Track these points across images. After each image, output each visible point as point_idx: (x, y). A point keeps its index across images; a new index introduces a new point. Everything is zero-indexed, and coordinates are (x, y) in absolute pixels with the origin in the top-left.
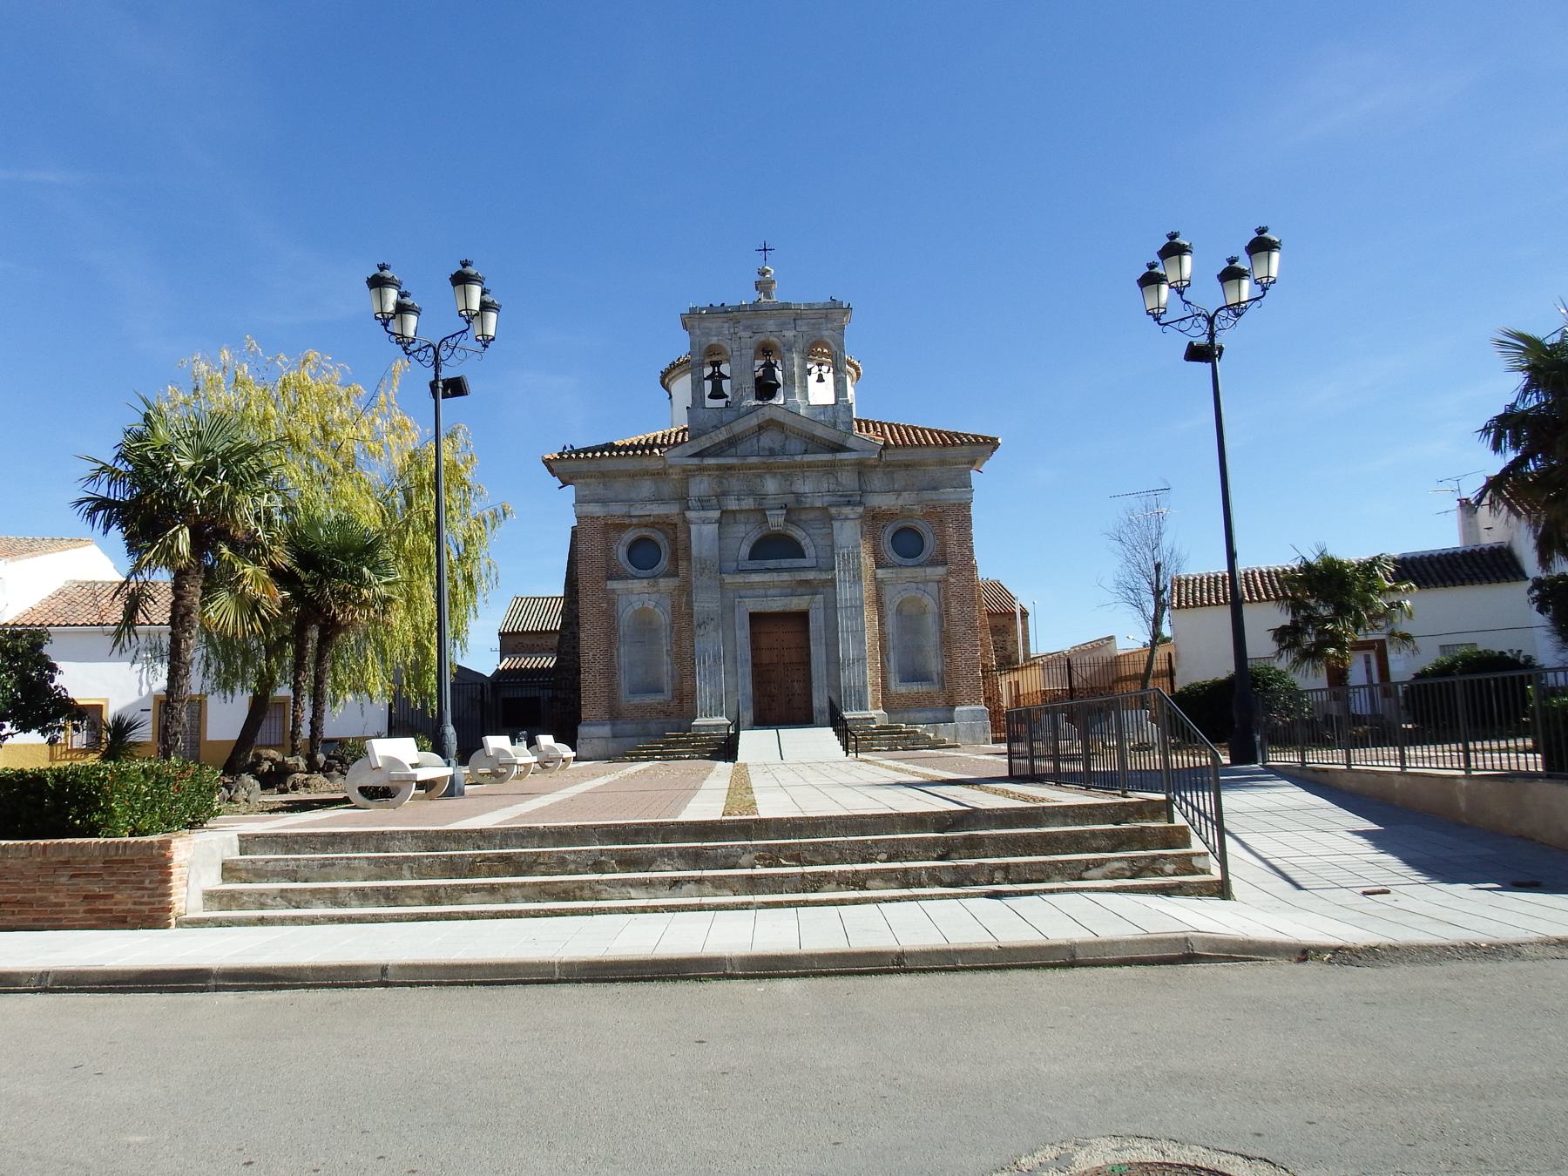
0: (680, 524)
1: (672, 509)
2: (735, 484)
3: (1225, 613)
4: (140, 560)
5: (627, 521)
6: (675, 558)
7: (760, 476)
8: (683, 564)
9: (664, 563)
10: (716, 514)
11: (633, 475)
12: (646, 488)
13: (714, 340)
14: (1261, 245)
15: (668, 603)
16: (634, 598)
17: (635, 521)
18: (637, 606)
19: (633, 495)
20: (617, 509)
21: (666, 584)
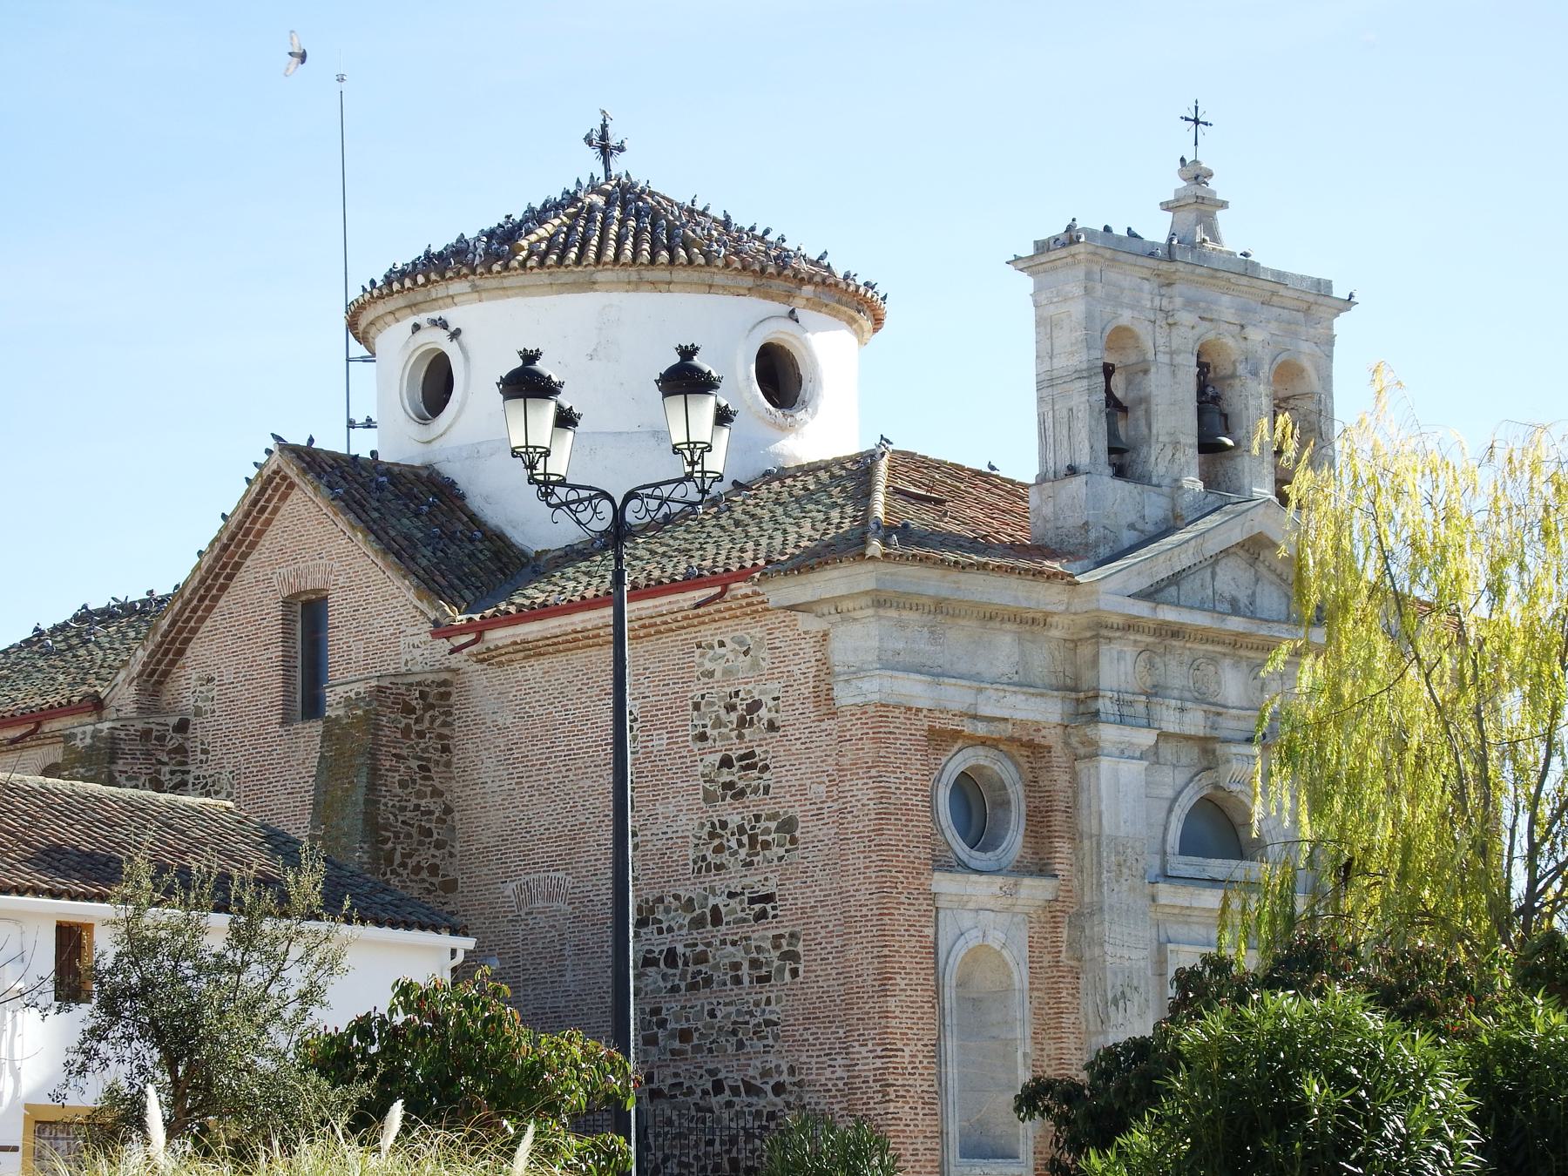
0: (1059, 754)
1: (1044, 712)
2: (1175, 674)
3: (608, 652)
4: (155, 679)
5: (968, 727)
6: (1040, 823)
7: (1213, 660)
8: (1063, 847)
9: (1015, 842)
10: (1146, 738)
11: (990, 616)
12: (1003, 651)
13: (1126, 317)
14: (341, 79)
15: (1022, 936)
16: (967, 920)
17: (981, 729)
18: (973, 938)
19: (981, 666)
20: (956, 696)
21: (1035, 890)
